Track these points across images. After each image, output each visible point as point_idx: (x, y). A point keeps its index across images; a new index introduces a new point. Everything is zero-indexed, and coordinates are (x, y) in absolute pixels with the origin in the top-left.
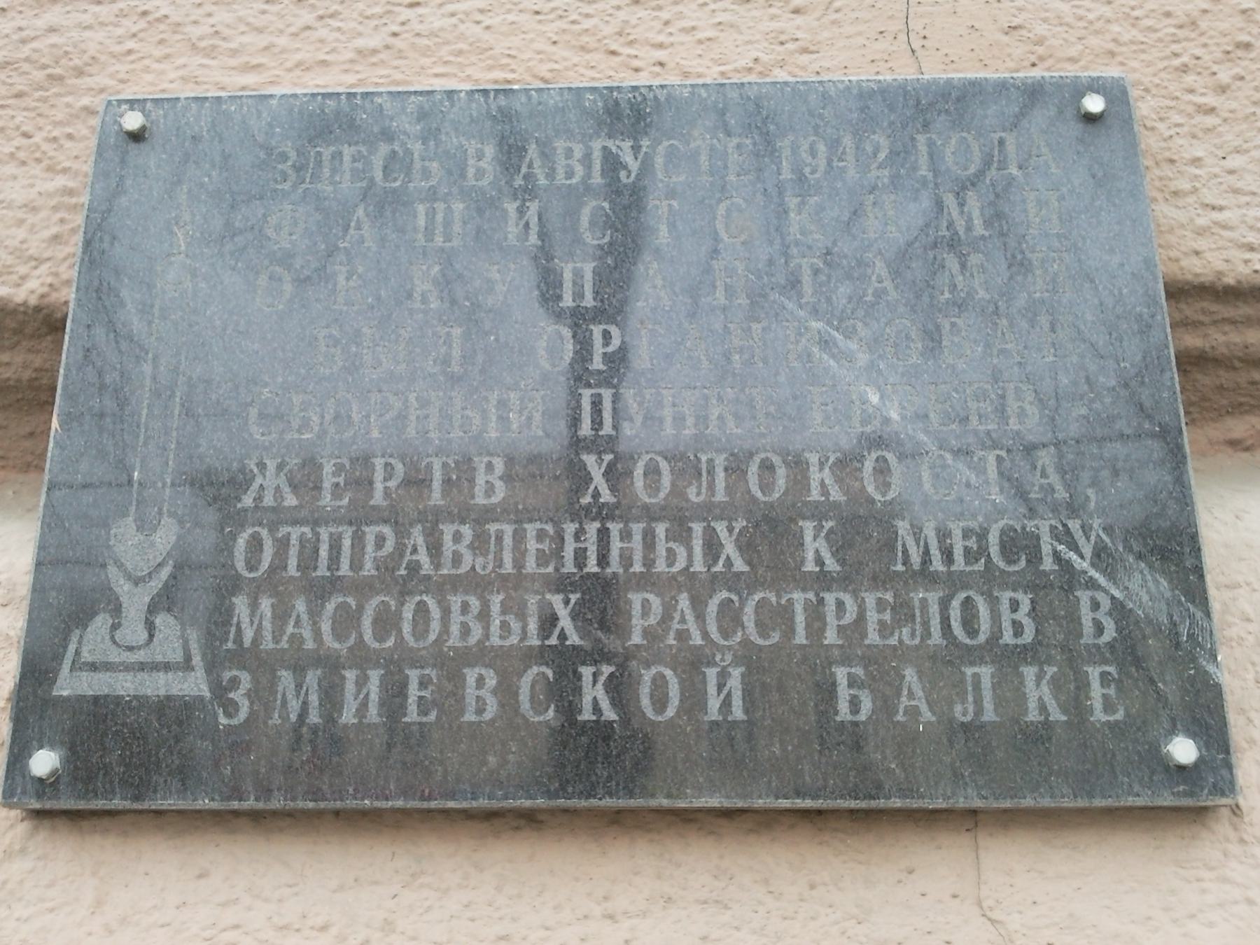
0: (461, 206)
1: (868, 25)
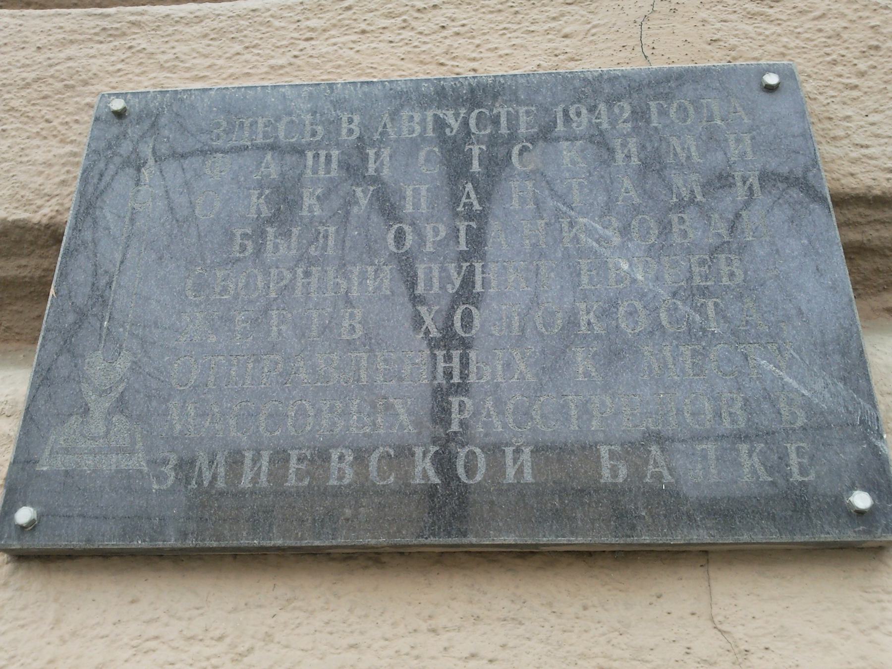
0: (337, 152)
1: (614, 42)
